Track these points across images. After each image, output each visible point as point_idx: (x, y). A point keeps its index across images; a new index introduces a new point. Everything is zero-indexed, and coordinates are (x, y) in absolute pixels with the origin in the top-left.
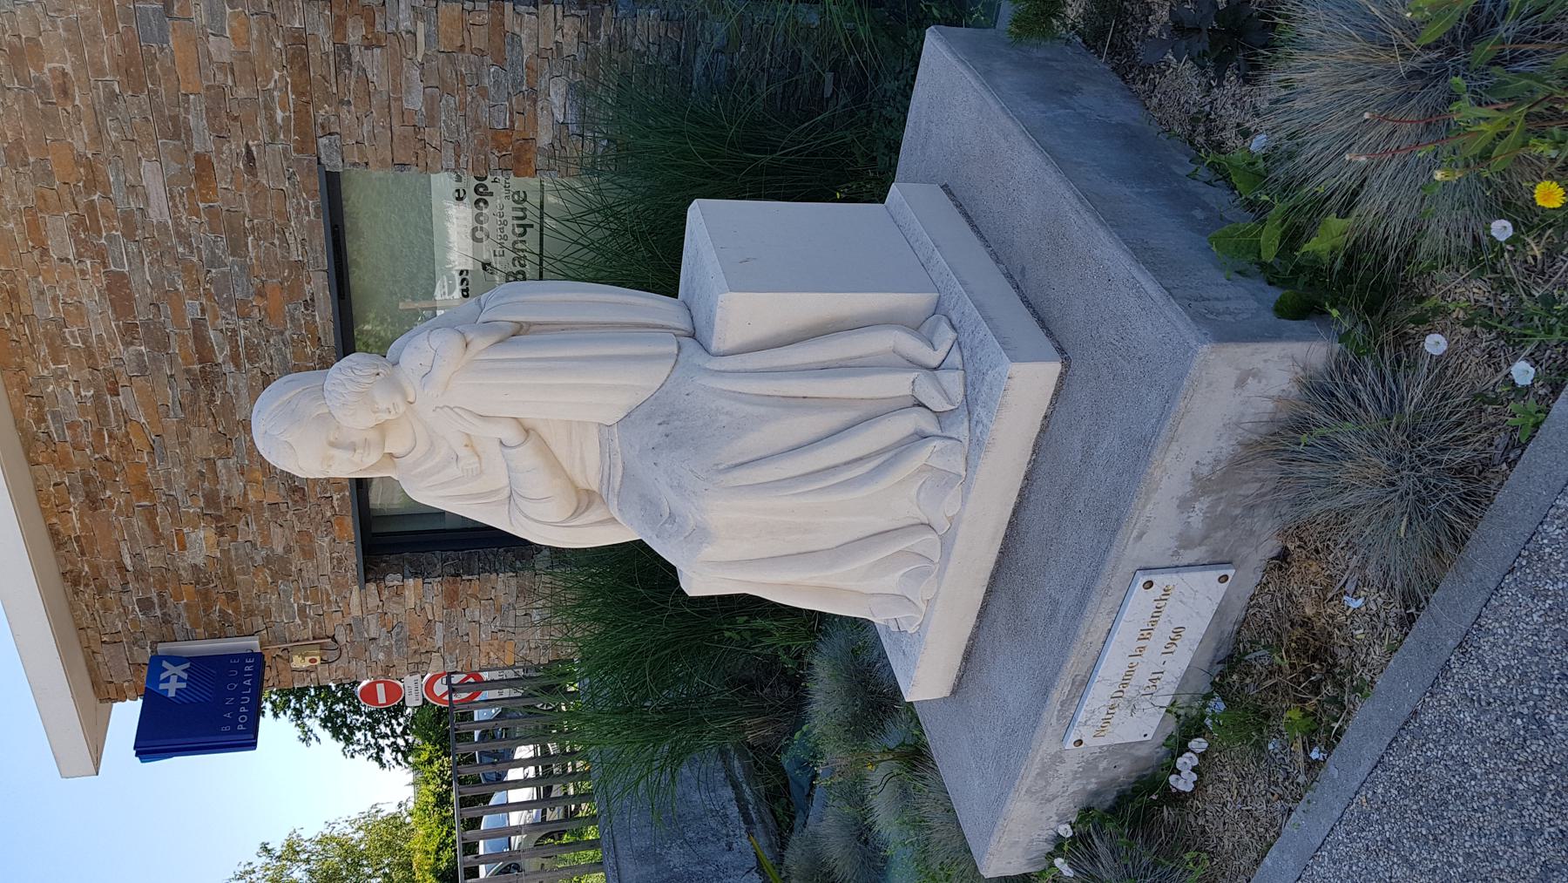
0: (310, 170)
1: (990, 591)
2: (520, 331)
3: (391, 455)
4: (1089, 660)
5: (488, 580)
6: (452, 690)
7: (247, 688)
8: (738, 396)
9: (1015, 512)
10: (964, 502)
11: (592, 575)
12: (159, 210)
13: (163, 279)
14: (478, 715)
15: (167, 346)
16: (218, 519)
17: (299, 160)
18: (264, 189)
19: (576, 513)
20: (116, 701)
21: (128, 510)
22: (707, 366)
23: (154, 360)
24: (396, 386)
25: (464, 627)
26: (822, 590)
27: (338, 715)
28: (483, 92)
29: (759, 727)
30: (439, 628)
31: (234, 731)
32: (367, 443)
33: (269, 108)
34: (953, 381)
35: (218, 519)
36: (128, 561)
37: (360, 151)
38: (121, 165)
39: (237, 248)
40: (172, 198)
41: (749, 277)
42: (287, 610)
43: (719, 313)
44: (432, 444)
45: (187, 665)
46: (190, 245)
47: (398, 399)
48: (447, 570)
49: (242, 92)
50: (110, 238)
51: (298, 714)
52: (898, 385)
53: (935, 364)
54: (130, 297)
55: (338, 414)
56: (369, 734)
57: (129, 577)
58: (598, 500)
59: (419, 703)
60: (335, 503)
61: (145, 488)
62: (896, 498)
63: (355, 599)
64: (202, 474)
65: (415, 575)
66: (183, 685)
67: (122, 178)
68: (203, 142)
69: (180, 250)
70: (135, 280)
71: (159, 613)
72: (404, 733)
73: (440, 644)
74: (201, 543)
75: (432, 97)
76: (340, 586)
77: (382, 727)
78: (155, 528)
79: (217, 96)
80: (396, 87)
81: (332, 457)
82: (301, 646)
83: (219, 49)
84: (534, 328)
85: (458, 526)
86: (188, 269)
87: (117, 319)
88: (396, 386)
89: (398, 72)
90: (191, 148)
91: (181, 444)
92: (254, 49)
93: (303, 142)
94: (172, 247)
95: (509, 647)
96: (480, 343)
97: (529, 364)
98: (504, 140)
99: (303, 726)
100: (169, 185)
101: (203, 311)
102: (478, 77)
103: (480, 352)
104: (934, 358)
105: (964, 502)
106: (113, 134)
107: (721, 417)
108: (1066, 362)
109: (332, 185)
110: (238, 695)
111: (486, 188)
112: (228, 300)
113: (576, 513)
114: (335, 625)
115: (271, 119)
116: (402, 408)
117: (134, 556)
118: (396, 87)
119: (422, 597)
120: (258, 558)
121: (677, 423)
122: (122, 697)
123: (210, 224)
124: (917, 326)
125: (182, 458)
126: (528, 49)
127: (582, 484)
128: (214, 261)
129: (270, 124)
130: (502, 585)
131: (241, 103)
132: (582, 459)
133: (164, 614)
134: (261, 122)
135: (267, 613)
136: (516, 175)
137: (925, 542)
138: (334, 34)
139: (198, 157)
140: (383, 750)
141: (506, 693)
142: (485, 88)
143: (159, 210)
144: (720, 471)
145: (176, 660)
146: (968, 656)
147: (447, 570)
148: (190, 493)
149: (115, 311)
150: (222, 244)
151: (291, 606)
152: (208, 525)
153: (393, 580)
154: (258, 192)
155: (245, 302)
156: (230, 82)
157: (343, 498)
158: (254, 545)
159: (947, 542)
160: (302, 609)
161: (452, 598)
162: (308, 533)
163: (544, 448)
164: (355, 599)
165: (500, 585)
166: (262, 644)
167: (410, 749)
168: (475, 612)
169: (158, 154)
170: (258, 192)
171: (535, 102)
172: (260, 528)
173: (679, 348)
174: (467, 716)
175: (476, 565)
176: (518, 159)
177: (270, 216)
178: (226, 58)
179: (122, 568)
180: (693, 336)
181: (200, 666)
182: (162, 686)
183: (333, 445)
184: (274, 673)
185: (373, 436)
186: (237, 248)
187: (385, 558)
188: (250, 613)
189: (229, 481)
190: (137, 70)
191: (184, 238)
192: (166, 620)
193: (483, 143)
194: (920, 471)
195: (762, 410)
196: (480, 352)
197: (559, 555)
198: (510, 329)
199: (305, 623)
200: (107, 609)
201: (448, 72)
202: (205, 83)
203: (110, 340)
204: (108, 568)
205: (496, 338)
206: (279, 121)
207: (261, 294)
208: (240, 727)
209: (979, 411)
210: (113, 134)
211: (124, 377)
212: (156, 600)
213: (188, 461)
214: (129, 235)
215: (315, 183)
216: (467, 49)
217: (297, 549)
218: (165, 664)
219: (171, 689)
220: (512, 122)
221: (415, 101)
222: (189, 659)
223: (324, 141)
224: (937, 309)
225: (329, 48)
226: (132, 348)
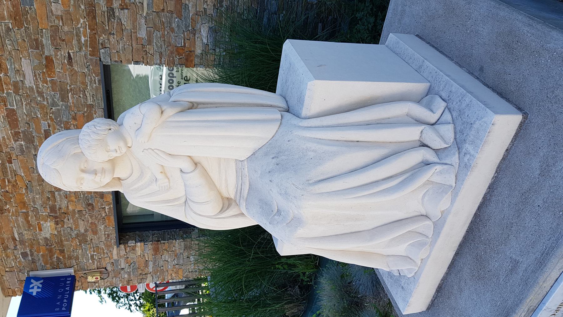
0: (96, 64)
1: (458, 254)
2: (193, 106)
3: (119, 179)
4: (540, 297)
5: (172, 243)
6: (157, 286)
7: (67, 291)
8: (320, 141)
9: (479, 208)
10: (453, 201)
11: (217, 241)
12: (29, 81)
13: (31, 112)
14: (167, 296)
15: (33, 142)
16: (56, 217)
17: (91, 59)
18: (76, 72)
19: (222, 210)
20: (12, 296)
21: (17, 214)
22: (300, 124)
23: (27, 148)
24: (120, 136)
25: (161, 263)
26: (363, 254)
27: (114, 292)
28: (172, 30)
29: (292, 309)
30: (151, 264)
31: (61, 310)
32: (103, 171)
33: (78, 36)
34: (448, 131)
35: (56, 217)
36: (16, 236)
37: (119, 56)
38: (13, 60)
39: (64, 98)
40: (35, 76)
41: (323, 72)
42: (86, 257)
43: (308, 93)
44: (142, 172)
45: (42, 281)
46: (43, 96)
47: (122, 144)
48: (154, 239)
49: (66, 28)
50: (8, 94)
51: (99, 292)
52: (412, 134)
53: (433, 121)
54: (17, 120)
55: (86, 152)
56: (126, 299)
57: (17, 243)
58: (234, 204)
59: (144, 291)
60: (107, 210)
61: (24, 204)
62: (410, 200)
63: (115, 251)
64: (49, 198)
65: (141, 241)
66: (40, 290)
67: (13, 67)
68: (49, 51)
69: (39, 99)
70: (19, 113)
71: (30, 258)
72: (139, 299)
73: (151, 270)
74: (49, 228)
75: (150, 32)
76: (109, 246)
77: (131, 297)
78: (28, 222)
79: (55, 30)
80: (134, 27)
81: (83, 178)
82: (92, 272)
83: (56, 9)
84: (200, 106)
85: (159, 219)
86: (42, 107)
87: (11, 130)
88: (120, 136)
89: (135, 20)
90: (44, 53)
91: (39, 185)
92: (71, 9)
93: (93, 51)
94: (35, 98)
95: (180, 272)
96: (170, 112)
97: (198, 124)
98: (181, 51)
99: (101, 297)
100: (34, 70)
101: (49, 126)
102: (170, 23)
103: (170, 117)
104: (433, 118)
105: (453, 201)
106: (9, 47)
107: (309, 153)
108: (525, 116)
109: (107, 71)
110: (63, 294)
111: (173, 74)
112: (60, 121)
113: (222, 210)
114: (106, 263)
115: (79, 41)
116: (124, 150)
117: (19, 234)
118: (134, 27)
119: (143, 251)
120: (73, 234)
121: (283, 157)
122: (14, 294)
123: (52, 87)
124: (424, 99)
125: (40, 191)
126: (192, 11)
127: (226, 195)
128: (54, 104)
129: (79, 43)
130: (178, 245)
131: (66, 33)
132: (226, 180)
133: (33, 259)
134: (75, 42)
135: (77, 258)
136: (186, 67)
137: (425, 226)
138: (107, 3)
139: (47, 58)
140: (131, 306)
141: (178, 287)
142: (173, 28)
143: (29, 81)
144: (310, 184)
145: (37, 279)
146: (440, 289)
147: (154, 239)
148: (43, 206)
149: (10, 126)
150: (58, 96)
151: (88, 255)
152: (51, 220)
153: (131, 243)
154: (74, 74)
155: (67, 123)
156: (61, 24)
157: (110, 208)
158: (71, 229)
159: (438, 226)
160: (92, 256)
161: (156, 251)
162: (95, 224)
163: (206, 174)
164: (115, 251)
165: (177, 245)
166: (75, 272)
167: (141, 305)
168: (166, 256)
169: (29, 56)
170: (74, 74)
171: (195, 35)
172: (74, 221)
173: (282, 116)
174: (163, 297)
175: (167, 236)
176: (187, 60)
177: (78, 84)
178: (59, 13)
179: (14, 239)
180: (288, 111)
181: (48, 282)
182: (30, 291)
183: (83, 171)
184: (80, 284)
185: (107, 166)
186: (64, 98)
187: (128, 234)
188: (70, 258)
189: (61, 201)
190: (20, 18)
191: (41, 94)
192: (33, 261)
193: (172, 53)
194: (424, 184)
195: (334, 149)
196: (170, 117)
197: (203, 232)
198: (188, 105)
199: (93, 262)
200: (8, 257)
201: (157, 20)
202: (50, 24)
203: (8, 139)
204: (8, 239)
205: (179, 109)
206: (83, 42)
207: (74, 118)
208: (64, 309)
209: (468, 147)
210: (9, 47)
211: (14, 155)
212: (29, 253)
213: (43, 192)
214: (16, 92)
215: (99, 70)
216: (165, 11)
217: (90, 230)
218: (32, 281)
219: (34, 291)
220: (185, 43)
221: (143, 34)
222: (43, 278)
223: (102, 51)
224: (429, 92)
225: (105, 9)
226: (18, 143)
